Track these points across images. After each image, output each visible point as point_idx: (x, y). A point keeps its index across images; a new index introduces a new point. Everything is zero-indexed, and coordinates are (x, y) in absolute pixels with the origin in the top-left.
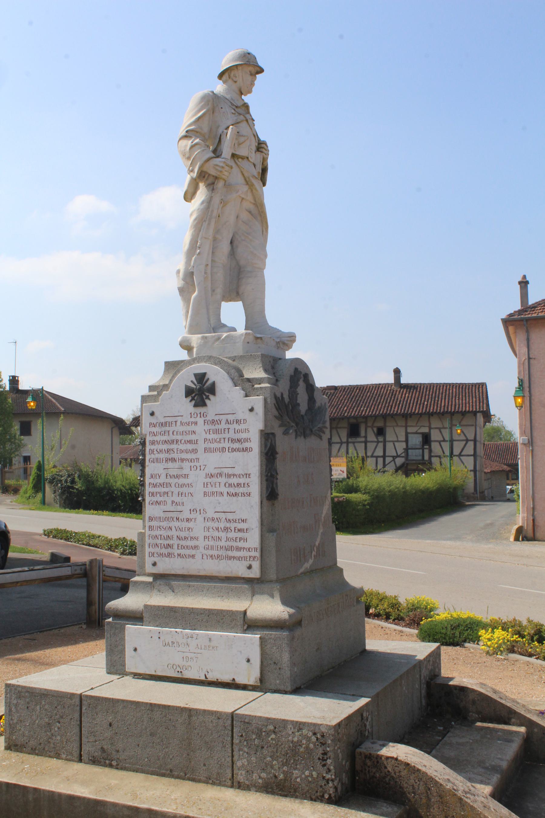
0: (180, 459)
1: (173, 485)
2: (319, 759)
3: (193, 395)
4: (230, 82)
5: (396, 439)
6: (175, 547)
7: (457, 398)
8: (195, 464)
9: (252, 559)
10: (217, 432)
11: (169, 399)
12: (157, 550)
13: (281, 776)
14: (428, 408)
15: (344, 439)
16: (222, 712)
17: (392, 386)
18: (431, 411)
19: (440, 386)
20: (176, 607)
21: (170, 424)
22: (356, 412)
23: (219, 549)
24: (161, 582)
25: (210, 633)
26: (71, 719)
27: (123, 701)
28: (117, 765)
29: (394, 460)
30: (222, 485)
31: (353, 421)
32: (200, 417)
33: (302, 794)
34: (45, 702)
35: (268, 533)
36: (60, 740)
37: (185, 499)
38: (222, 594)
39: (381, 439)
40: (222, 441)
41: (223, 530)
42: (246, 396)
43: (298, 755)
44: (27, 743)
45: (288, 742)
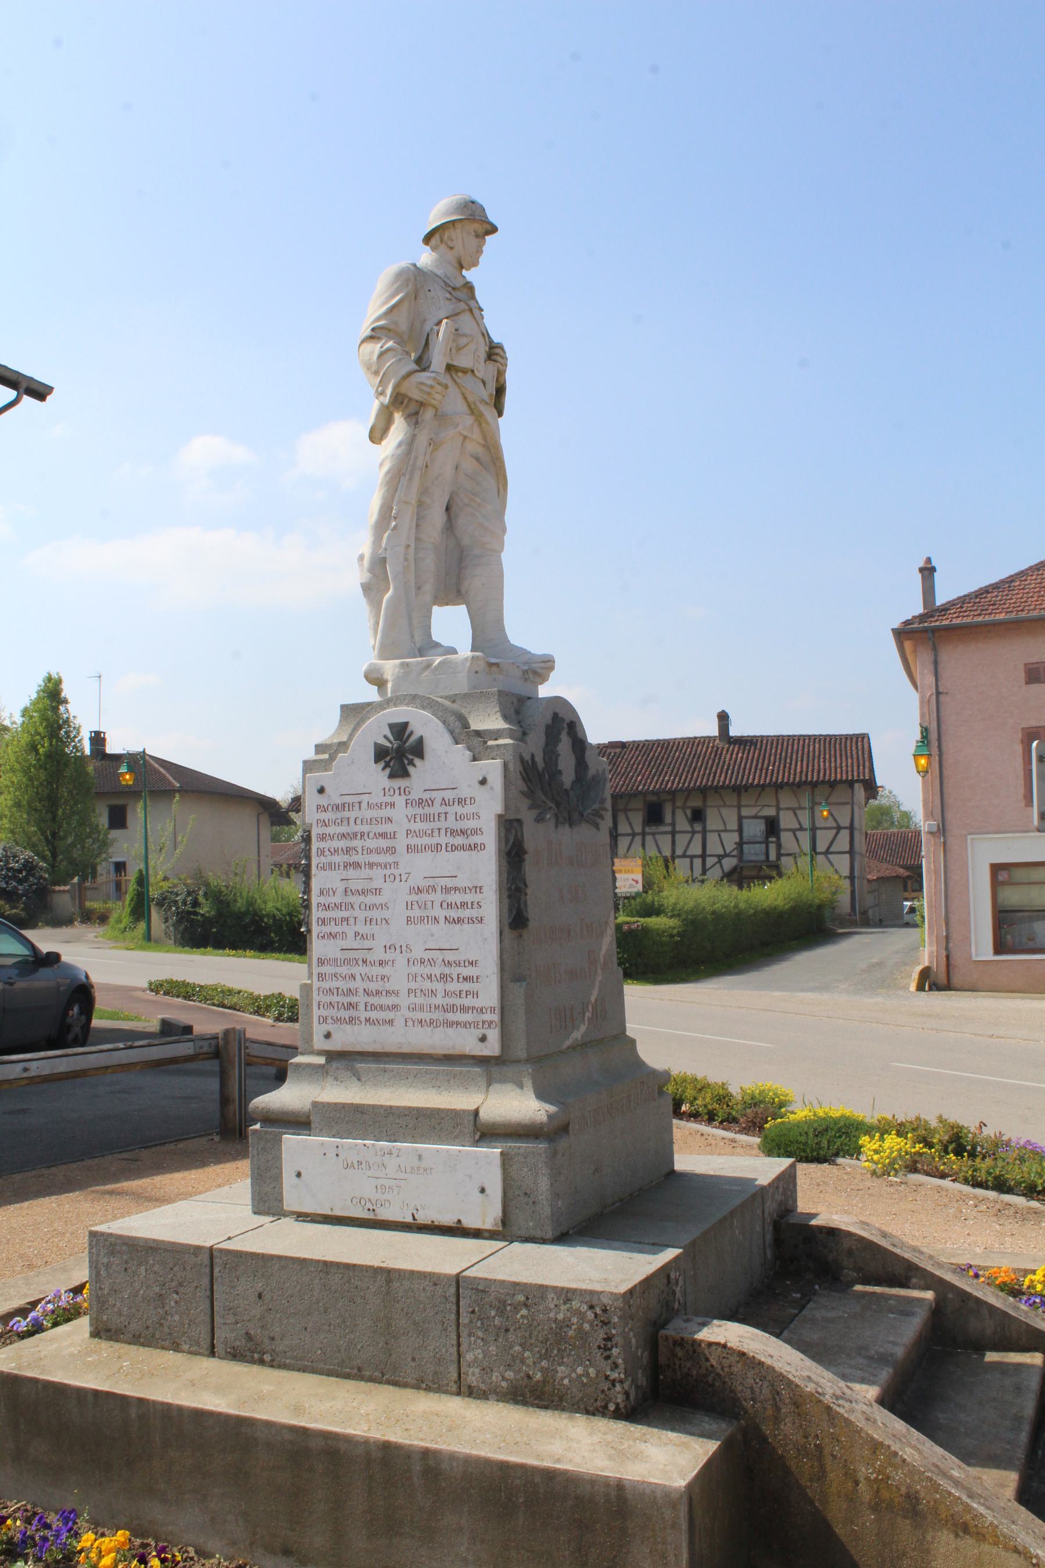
1: (356, 906)
2: (599, 1347)
3: (388, 759)
4: (443, 247)
6: (362, 1007)
7: (822, 760)
8: (393, 871)
9: (486, 1026)
10: (426, 818)
13: (538, 1376)
14: (775, 775)
15: (638, 829)
16: (441, 1274)
18: (780, 780)
19: (794, 740)
20: (364, 1105)
21: (350, 806)
22: (657, 783)
23: (433, 1009)
26: (197, 1287)
28: (273, 1360)
29: (720, 862)
30: (437, 904)
33: (573, 1405)
37: (375, 929)
39: (698, 827)
40: (436, 833)
43: (566, 1342)
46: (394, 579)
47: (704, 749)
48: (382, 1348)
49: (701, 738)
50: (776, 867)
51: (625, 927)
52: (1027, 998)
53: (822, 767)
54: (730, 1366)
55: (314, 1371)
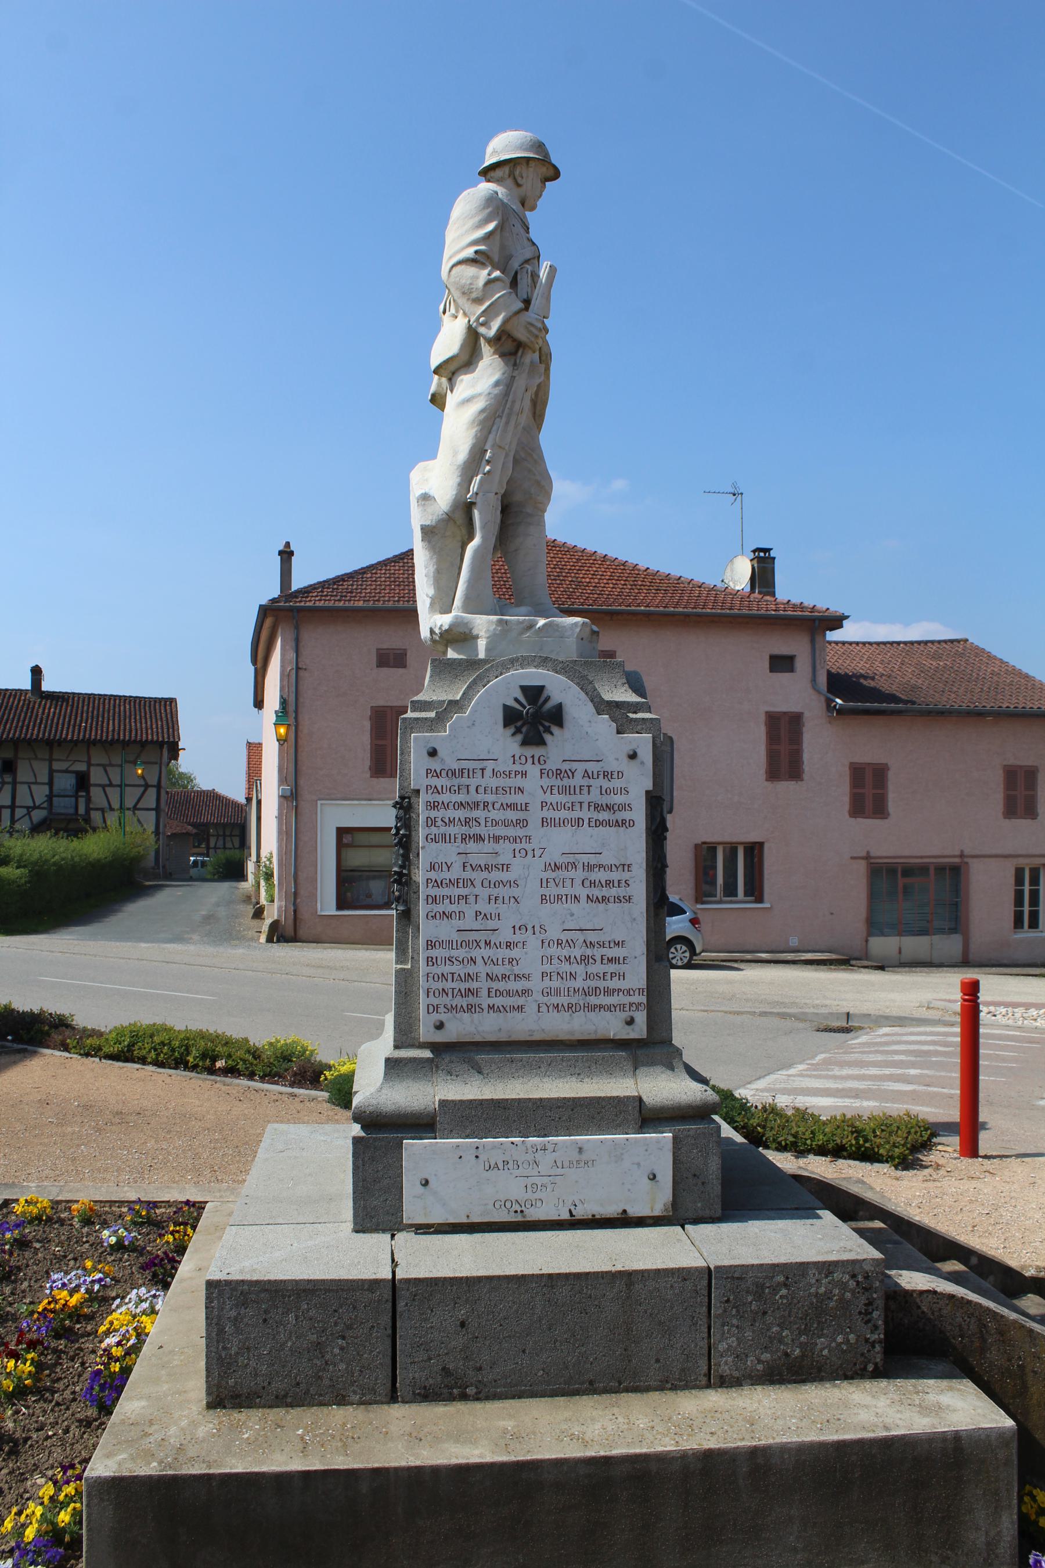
0: (491, 836)
1: (478, 883)
2: (860, 1313)
3: (519, 724)
4: (510, 182)
5: (33, 780)
6: (485, 992)
7: (133, 720)
8: (524, 845)
10: (565, 790)
11: (469, 727)
12: (447, 1000)
14: (88, 732)
16: (691, 1268)
17: (26, 694)
18: (93, 737)
19: (105, 699)
20: (507, 1100)
23: (571, 993)
24: (453, 1058)
26: (373, 1327)
27: (567, 1276)
29: (29, 813)
30: (578, 882)
32: (533, 763)
33: (832, 1373)
34: (308, 1304)
36: (346, 1369)
37: (502, 908)
38: (577, 1071)
40: (577, 807)
41: (579, 960)
42: (618, 732)
46: (483, 527)
47: (16, 702)
48: (621, 1355)
50: (87, 819)
52: (334, 948)
54: (940, 1309)
55: (533, 1395)
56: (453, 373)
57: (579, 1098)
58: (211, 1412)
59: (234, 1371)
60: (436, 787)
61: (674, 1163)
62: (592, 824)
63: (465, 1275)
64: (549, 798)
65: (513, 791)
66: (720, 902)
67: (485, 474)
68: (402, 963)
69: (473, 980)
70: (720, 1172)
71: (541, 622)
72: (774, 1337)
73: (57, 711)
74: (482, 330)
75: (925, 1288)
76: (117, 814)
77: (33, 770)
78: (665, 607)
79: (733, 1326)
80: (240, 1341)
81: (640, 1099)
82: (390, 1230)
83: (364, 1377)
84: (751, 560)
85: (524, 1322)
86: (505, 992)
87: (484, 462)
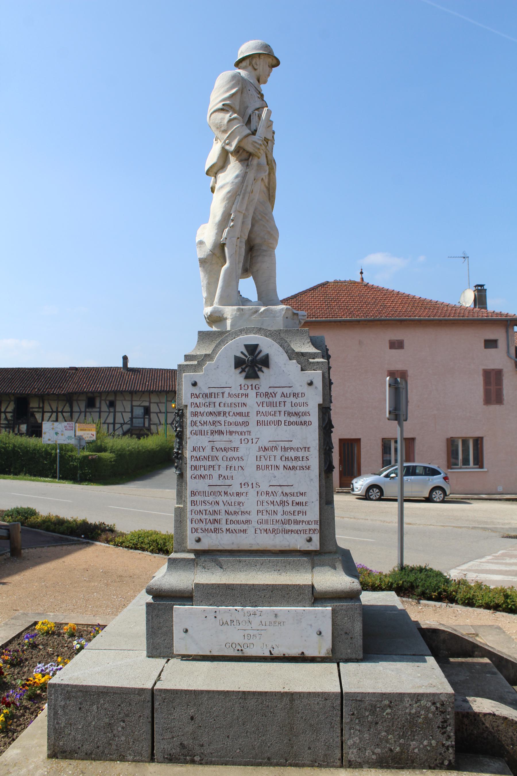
0: (228, 431)
1: (220, 458)
2: (439, 727)
3: (244, 366)
4: (250, 68)
5: (123, 410)
6: (224, 521)
7: (171, 381)
8: (247, 436)
9: (312, 532)
10: (271, 404)
12: (203, 526)
13: (398, 749)
14: (149, 387)
15: (83, 409)
16: (330, 692)
18: (152, 389)
19: (158, 371)
20: (234, 584)
21: (216, 395)
22: (93, 388)
23: (275, 523)
24: (206, 559)
25: (276, 609)
26: (140, 716)
27: (254, 693)
28: (201, 760)
29: (122, 426)
30: (278, 458)
31: (90, 395)
33: (421, 764)
34: (104, 700)
35: (327, 506)
36: (125, 740)
37: (234, 473)
39: (112, 410)
41: (279, 504)
42: (302, 370)
43: (416, 727)
44: (79, 748)
45: (405, 715)
46: (230, 257)
47: (116, 373)
48: (287, 743)
49: (114, 367)
50: (149, 429)
51: (90, 457)
53: (171, 384)
54: (498, 726)
55: (234, 764)
56: (216, 174)
57: (276, 585)
58: (50, 760)
59: (63, 737)
60: (196, 403)
61: (333, 625)
62: (286, 424)
63: (193, 689)
64: (261, 409)
65: (240, 405)
66: (461, 468)
67: (231, 227)
68: (180, 504)
69: (217, 514)
70: (361, 631)
71: (263, 309)
72: (383, 739)
73: (135, 377)
74: (227, 147)
75: (488, 711)
76: (164, 426)
77: (123, 406)
78: (428, 317)
79: (356, 730)
80: (66, 720)
81: (313, 586)
82: (167, 657)
83: (135, 746)
84: (474, 291)
85: (229, 719)
86: (236, 522)
87: (230, 220)
